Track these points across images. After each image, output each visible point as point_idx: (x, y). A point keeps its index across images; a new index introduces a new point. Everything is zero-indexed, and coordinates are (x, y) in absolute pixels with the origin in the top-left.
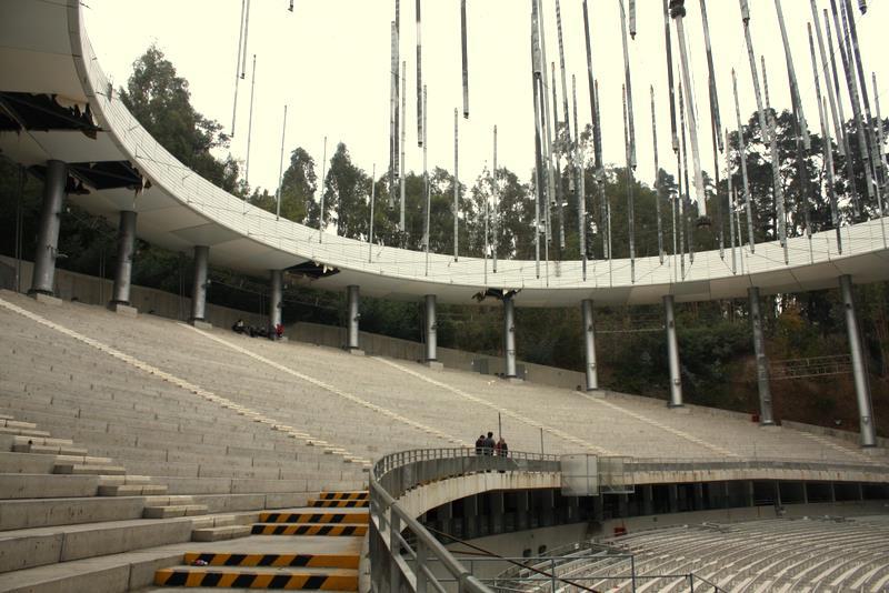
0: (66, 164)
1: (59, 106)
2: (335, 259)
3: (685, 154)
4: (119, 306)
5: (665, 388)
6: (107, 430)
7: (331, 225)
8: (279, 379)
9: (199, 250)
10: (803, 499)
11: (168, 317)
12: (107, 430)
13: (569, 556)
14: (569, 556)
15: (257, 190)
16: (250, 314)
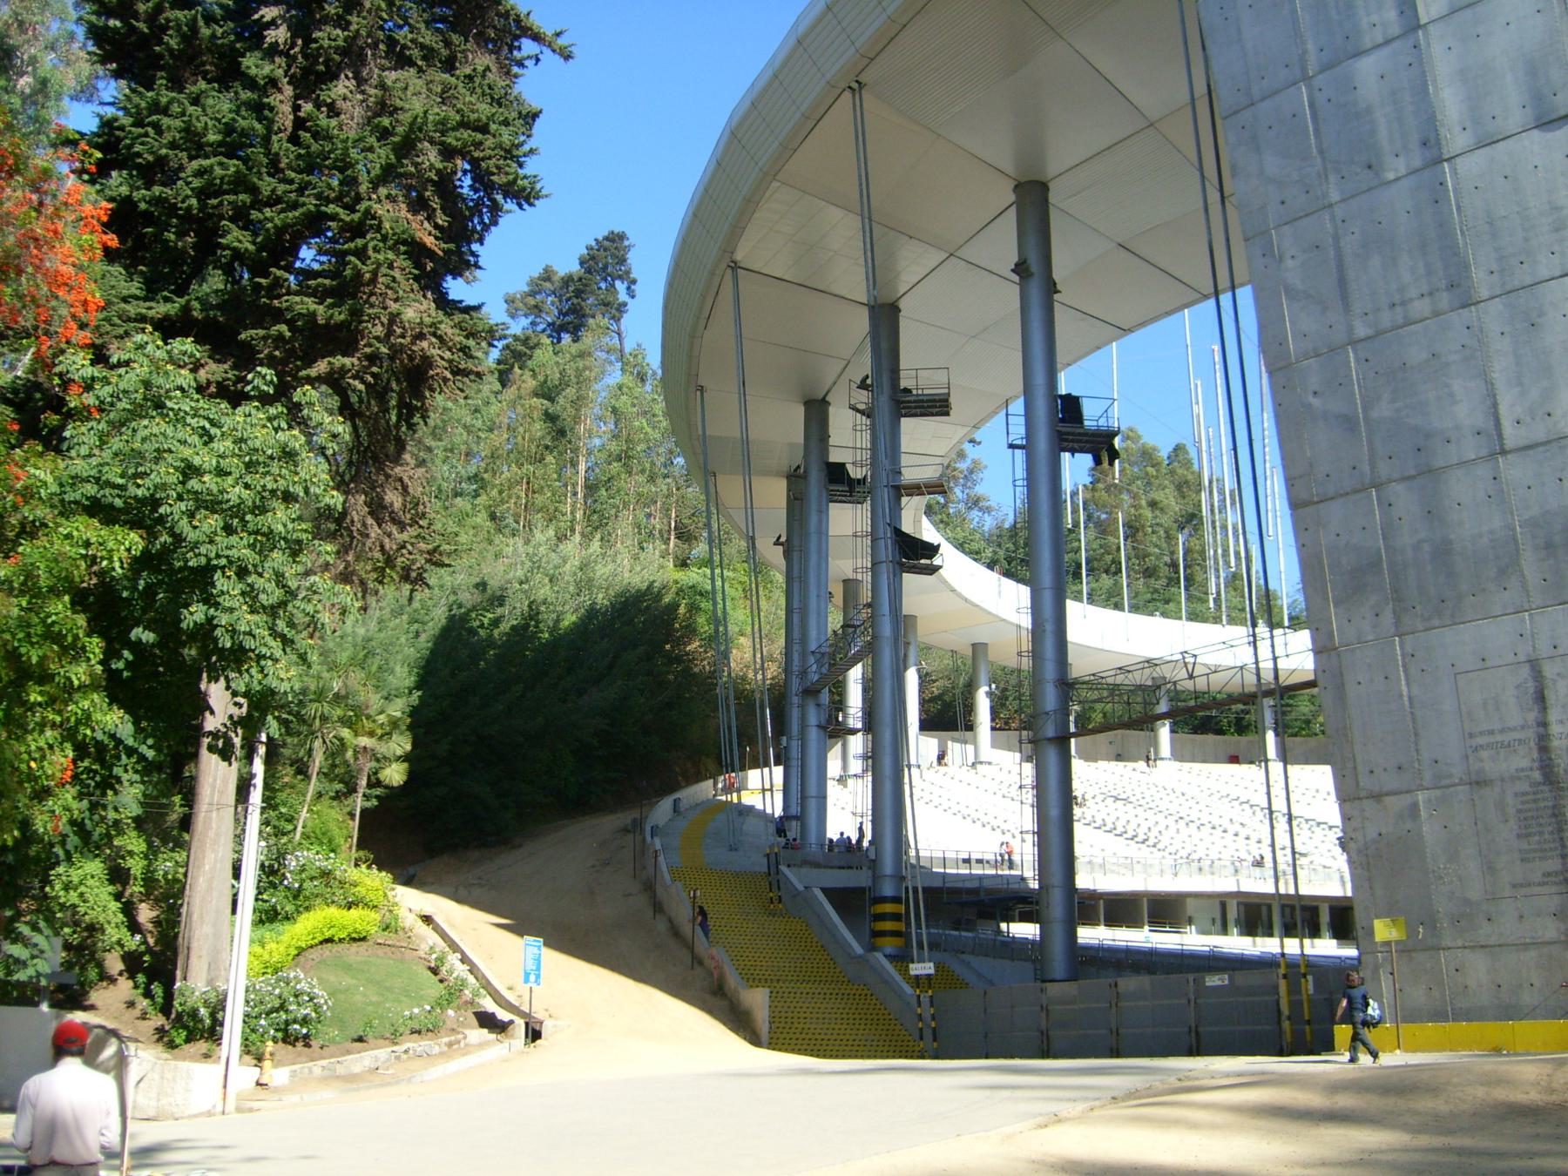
0: (80, 1053)
1: (1350, 862)
2: (452, 926)
3: (1045, 1099)
4: (850, 782)
5: (1045, 1035)
6: (1033, 198)
7: (214, 462)
8: (1301, 861)
9: (978, 649)
10: (1270, 927)
11: (710, 182)
12: (1033, 198)
13: (256, 796)
14: (256, 796)
15: (558, 621)
16: (832, 789)
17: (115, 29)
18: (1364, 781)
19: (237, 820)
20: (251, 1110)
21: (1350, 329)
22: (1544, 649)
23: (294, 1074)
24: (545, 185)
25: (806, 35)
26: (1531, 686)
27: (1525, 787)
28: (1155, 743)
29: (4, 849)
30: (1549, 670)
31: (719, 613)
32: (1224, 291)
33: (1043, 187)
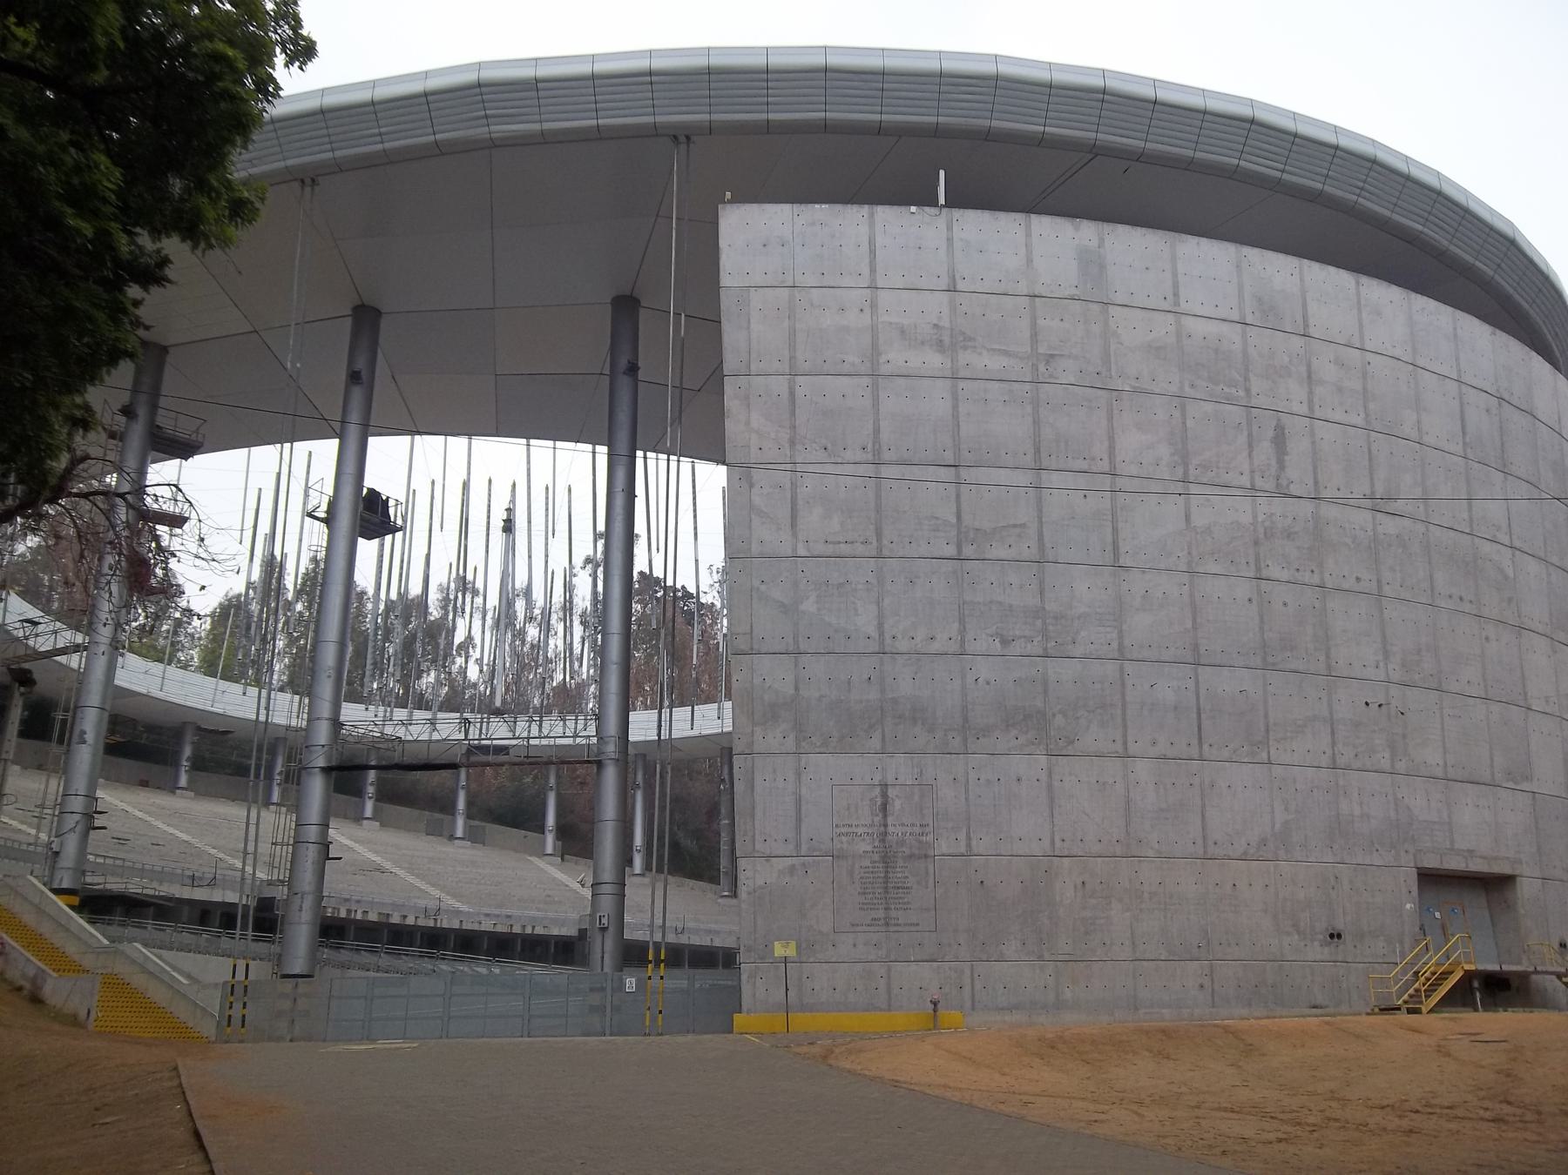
17: (227, 12)
18: (1270, 659)
19: (571, 602)
20: (1052, 1048)
21: (795, 550)
22: (890, 780)
23: (1092, 265)
24: (2, 669)
25: (1164, 104)
26: (879, 801)
27: (867, 863)
28: (177, 778)
29: (8, 851)
30: (891, 792)
31: (277, 553)
32: (958, 475)
33: (376, 314)
